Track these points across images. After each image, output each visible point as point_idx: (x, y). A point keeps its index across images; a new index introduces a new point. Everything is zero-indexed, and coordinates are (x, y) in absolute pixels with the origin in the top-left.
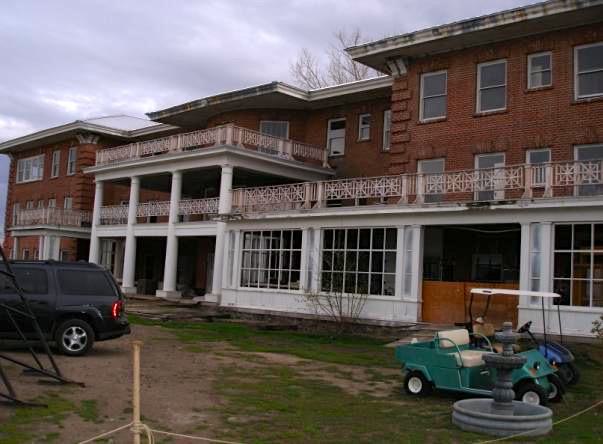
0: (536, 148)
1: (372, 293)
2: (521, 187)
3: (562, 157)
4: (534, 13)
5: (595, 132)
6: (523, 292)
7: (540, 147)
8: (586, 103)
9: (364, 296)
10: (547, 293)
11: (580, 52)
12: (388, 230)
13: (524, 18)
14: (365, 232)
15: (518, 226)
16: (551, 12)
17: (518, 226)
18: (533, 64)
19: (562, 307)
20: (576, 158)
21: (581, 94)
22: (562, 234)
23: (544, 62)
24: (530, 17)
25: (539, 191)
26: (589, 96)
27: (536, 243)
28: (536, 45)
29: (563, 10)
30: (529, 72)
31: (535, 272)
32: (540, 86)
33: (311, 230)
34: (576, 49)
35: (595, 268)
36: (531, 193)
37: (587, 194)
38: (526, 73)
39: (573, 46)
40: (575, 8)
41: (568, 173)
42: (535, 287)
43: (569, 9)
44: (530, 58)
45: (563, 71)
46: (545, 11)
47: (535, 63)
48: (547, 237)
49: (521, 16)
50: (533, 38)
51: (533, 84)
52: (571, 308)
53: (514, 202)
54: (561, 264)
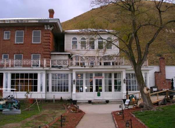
0: (5, 54)
1: (34, 91)
2: (38, 64)
3: (11, 58)
4: (7, 22)
5: (19, 51)
6: (4, 89)
7: (6, 54)
8: (17, 44)
9: (32, 92)
10: (9, 89)
11: (34, 32)
12: (16, 74)
13: (5, 22)
14: (18, 74)
15: (3, 73)
16: (11, 22)
17: (3, 73)
18: (5, 33)
19: (17, 92)
20: (32, 59)
21: (33, 42)
22: (13, 76)
23: (8, 33)
24: (6, 22)
25: (8, 66)
26: (19, 43)
27: (7, 77)
28: (6, 29)
29: (14, 22)
30: (4, 35)
31: (7, 84)
32: (6, 39)
33: (7, 73)
34: (16, 31)
35: (20, 83)
36: (6, 66)
37: (24, 67)
38: (4, 35)
39: (16, 30)
40: (17, 22)
41: (30, 62)
42: (7, 87)
43: (16, 22)
44: (5, 31)
45: (13, 36)
46: (10, 22)
47: (6, 33)
48: (9, 76)
49: (4, 22)
50: (6, 27)
51: (5, 38)
52: (19, 92)
53: (2, 68)
54: (13, 83)
